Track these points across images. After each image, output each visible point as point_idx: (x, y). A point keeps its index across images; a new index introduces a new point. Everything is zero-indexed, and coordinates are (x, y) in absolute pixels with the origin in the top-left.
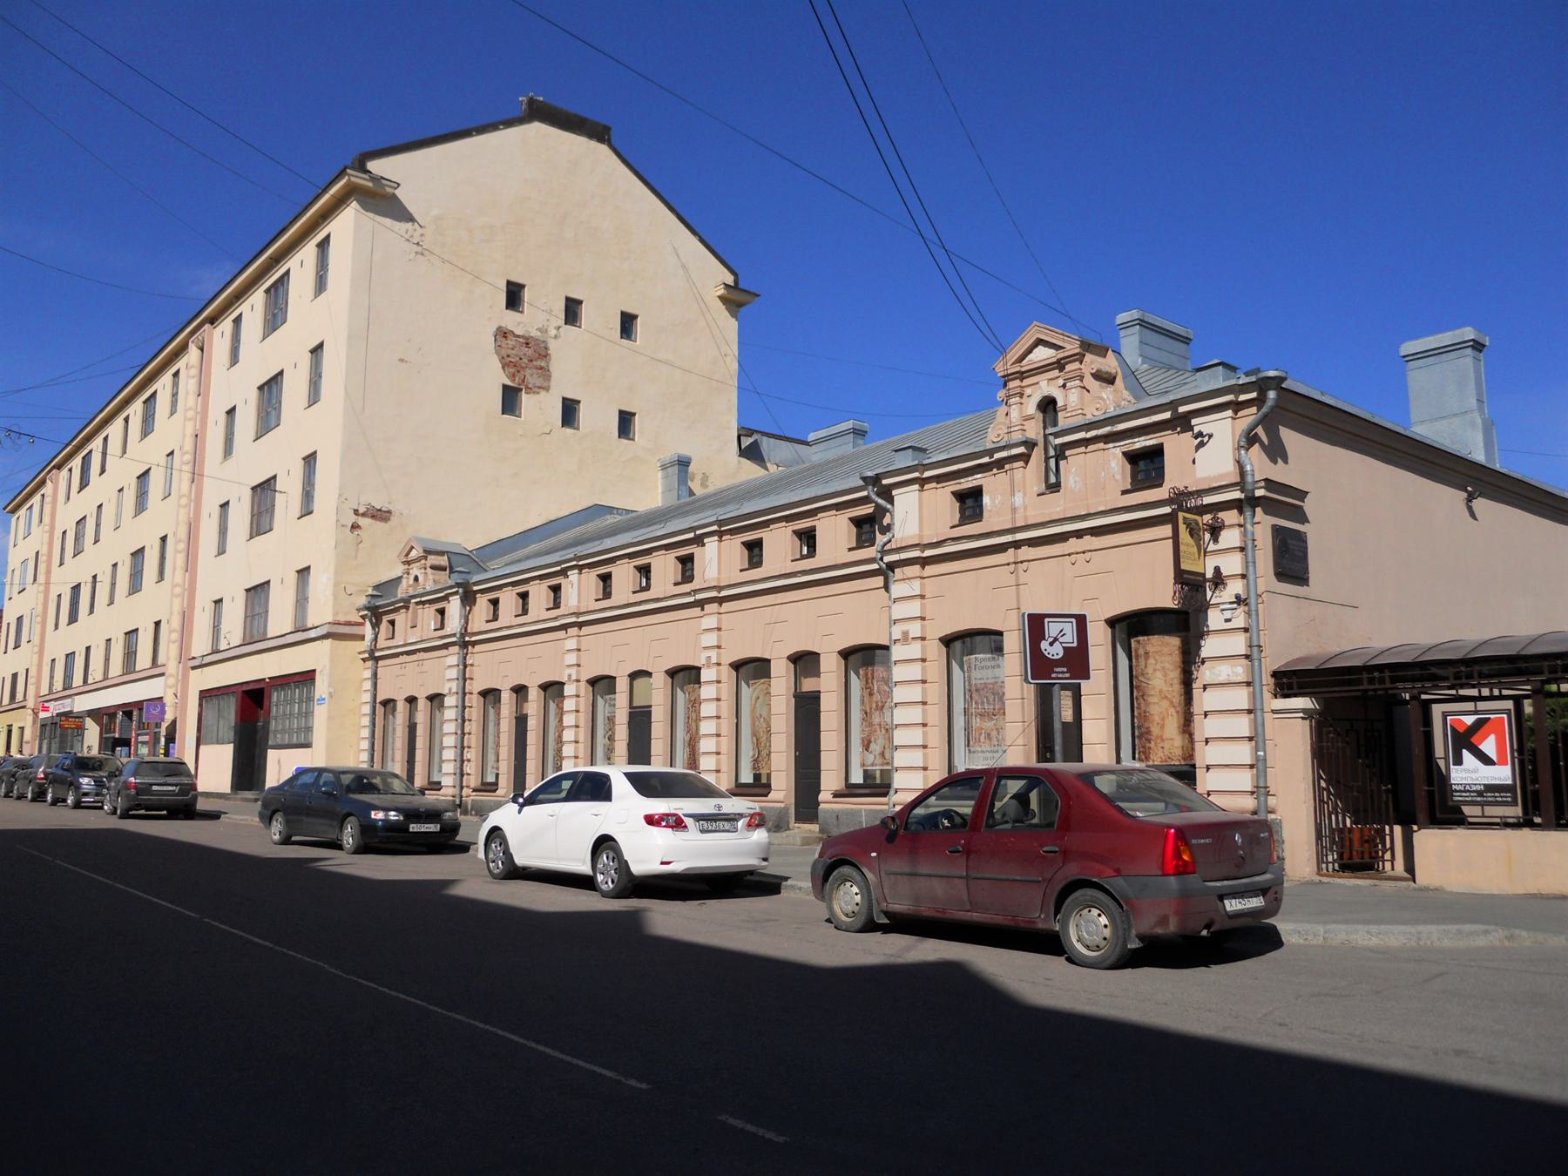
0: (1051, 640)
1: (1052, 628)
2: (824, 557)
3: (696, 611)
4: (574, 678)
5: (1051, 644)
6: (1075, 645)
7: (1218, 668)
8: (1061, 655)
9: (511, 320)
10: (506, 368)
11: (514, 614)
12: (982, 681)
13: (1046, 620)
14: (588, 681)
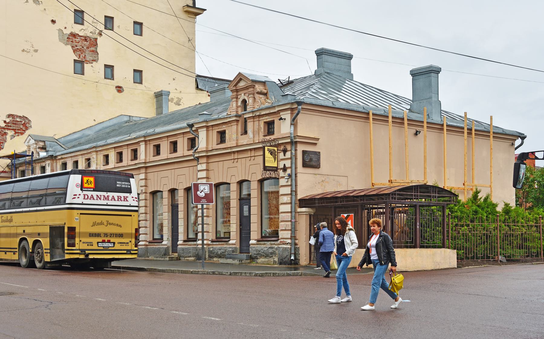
0: (201, 191)
1: (201, 188)
2: (179, 153)
3: (195, 163)
4: (144, 191)
5: (201, 192)
6: (209, 192)
7: (284, 198)
8: (204, 195)
9: (77, 29)
10: (75, 52)
11: (263, 135)
12: (227, 201)
13: (199, 185)
14: (151, 193)
